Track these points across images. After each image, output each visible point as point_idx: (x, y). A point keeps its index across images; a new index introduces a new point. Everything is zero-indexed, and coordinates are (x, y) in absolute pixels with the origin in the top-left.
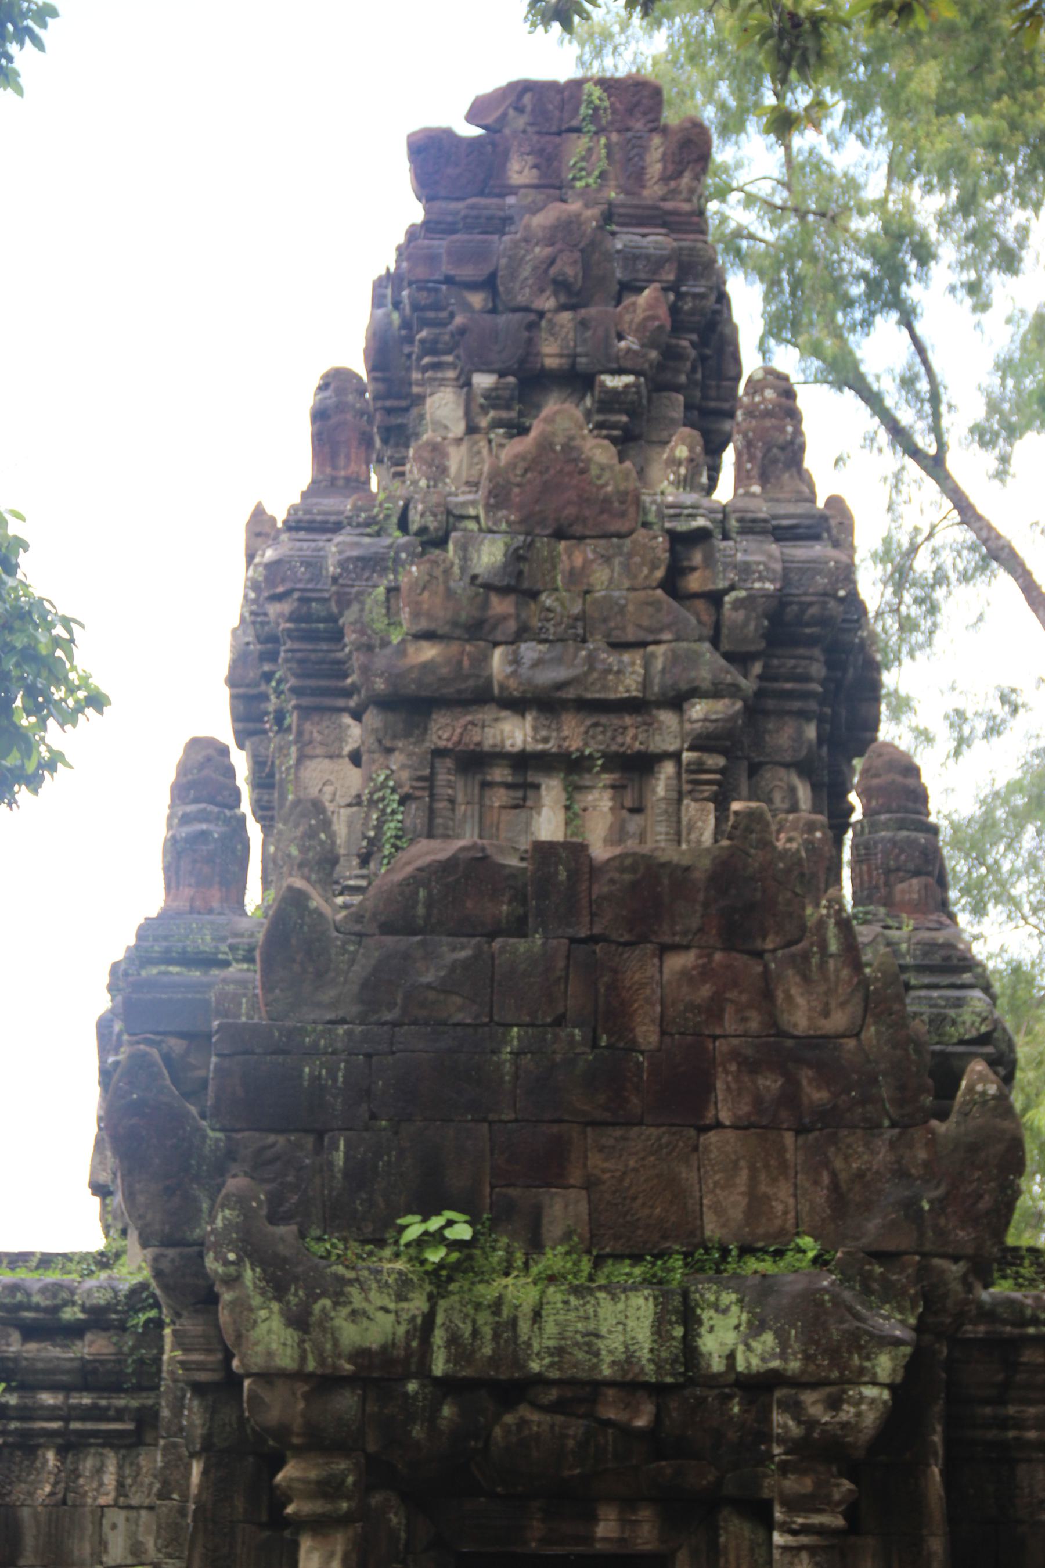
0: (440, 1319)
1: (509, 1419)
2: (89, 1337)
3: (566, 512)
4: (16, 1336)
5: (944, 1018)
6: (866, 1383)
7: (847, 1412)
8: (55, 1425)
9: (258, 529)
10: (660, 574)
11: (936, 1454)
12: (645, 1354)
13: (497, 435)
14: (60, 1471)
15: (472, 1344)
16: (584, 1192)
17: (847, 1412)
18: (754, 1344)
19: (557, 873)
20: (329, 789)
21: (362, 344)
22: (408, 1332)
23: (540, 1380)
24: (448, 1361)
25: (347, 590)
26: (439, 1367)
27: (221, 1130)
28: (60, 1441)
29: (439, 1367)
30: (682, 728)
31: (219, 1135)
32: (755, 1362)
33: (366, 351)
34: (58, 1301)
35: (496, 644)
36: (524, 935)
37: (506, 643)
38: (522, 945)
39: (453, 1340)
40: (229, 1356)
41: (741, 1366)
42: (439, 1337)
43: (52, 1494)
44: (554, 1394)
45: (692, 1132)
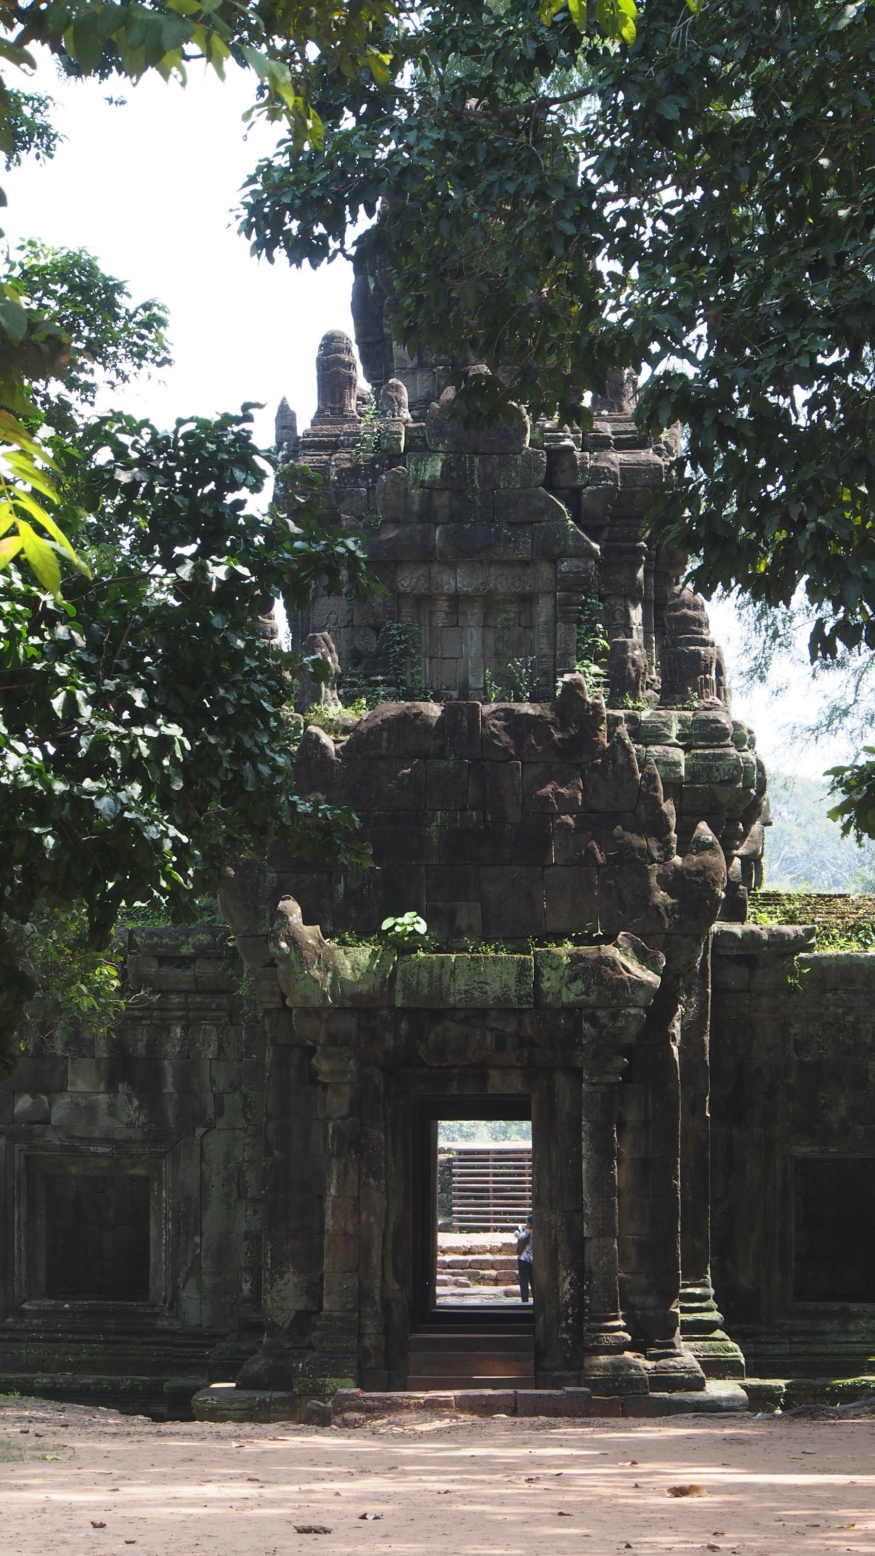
0: (399, 977)
1: (439, 1028)
2: (198, 963)
3: (360, 987)
4: (155, 963)
5: (711, 768)
6: (631, 1007)
7: (621, 1023)
8: (180, 1014)
9: (283, 423)
10: (542, 477)
11: (674, 1040)
12: (513, 993)
13: (438, 370)
14: (185, 1039)
15: (417, 989)
16: (479, 904)
17: (621, 1023)
18: (571, 986)
19: (462, 721)
20: (333, 616)
21: (349, 298)
22: (382, 983)
23: (454, 1009)
24: (404, 998)
25: (343, 490)
26: (399, 1002)
27: (276, 872)
28: (183, 1022)
29: (399, 1002)
30: (556, 576)
31: (275, 875)
32: (572, 996)
33: (352, 304)
34: (178, 942)
35: (437, 524)
36: (444, 758)
37: (444, 523)
38: (443, 764)
39: (406, 987)
40: (284, 997)
41: (564, 999)
42: (398, 986)
43: (180, 1052)
44: (462, 1014)
45: (540, 869)
